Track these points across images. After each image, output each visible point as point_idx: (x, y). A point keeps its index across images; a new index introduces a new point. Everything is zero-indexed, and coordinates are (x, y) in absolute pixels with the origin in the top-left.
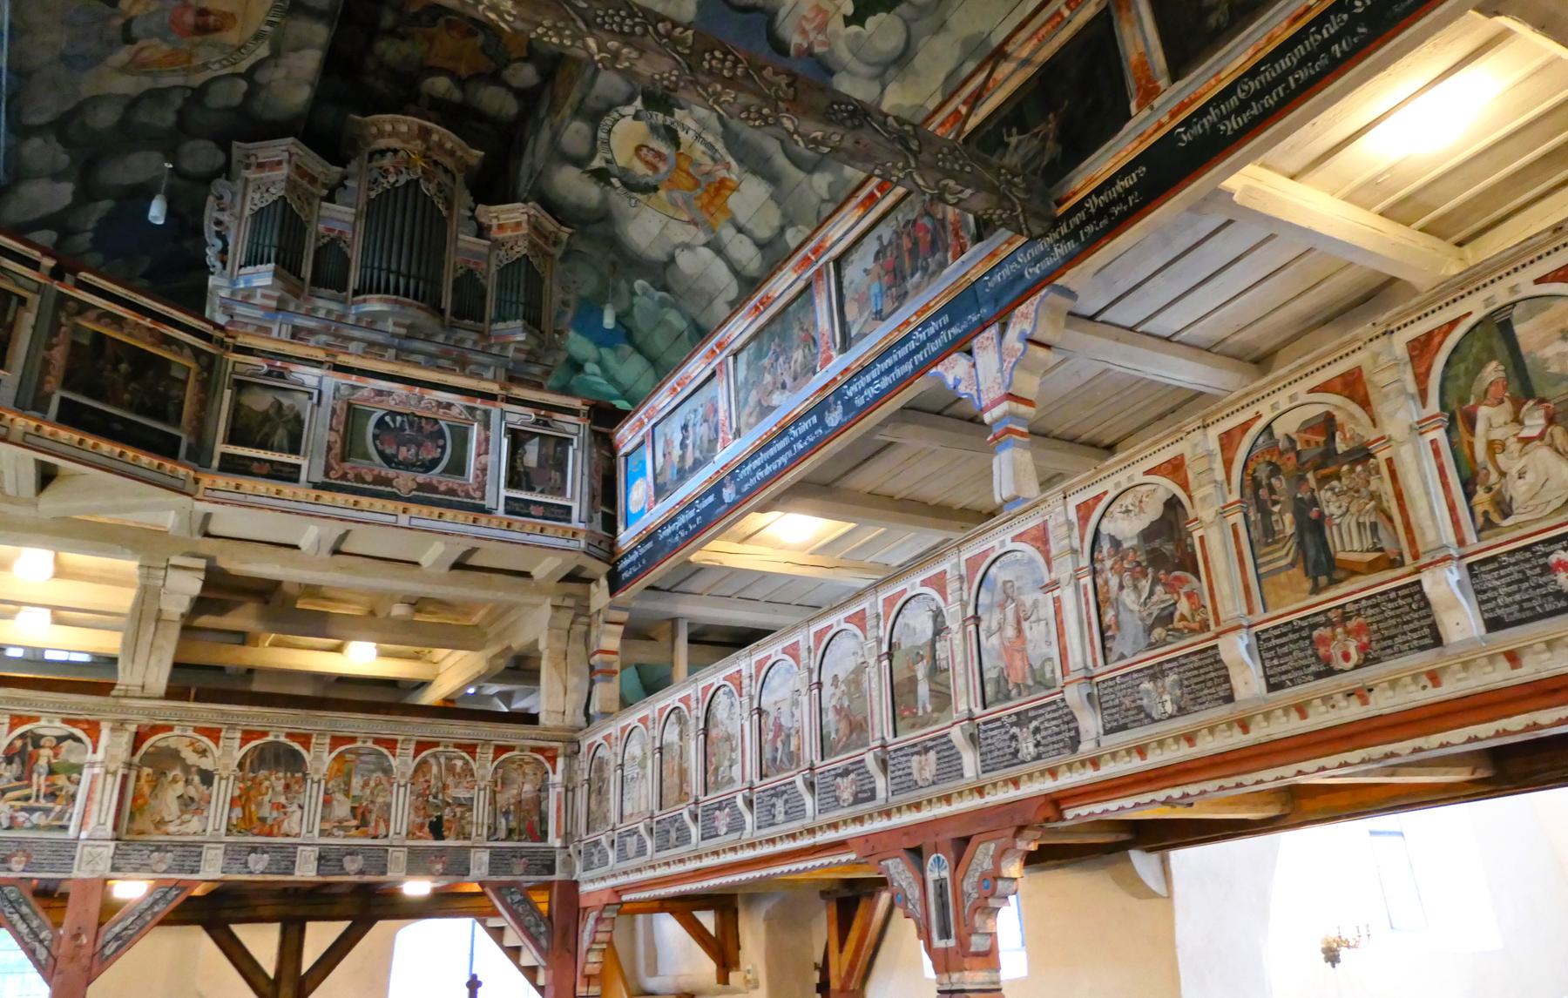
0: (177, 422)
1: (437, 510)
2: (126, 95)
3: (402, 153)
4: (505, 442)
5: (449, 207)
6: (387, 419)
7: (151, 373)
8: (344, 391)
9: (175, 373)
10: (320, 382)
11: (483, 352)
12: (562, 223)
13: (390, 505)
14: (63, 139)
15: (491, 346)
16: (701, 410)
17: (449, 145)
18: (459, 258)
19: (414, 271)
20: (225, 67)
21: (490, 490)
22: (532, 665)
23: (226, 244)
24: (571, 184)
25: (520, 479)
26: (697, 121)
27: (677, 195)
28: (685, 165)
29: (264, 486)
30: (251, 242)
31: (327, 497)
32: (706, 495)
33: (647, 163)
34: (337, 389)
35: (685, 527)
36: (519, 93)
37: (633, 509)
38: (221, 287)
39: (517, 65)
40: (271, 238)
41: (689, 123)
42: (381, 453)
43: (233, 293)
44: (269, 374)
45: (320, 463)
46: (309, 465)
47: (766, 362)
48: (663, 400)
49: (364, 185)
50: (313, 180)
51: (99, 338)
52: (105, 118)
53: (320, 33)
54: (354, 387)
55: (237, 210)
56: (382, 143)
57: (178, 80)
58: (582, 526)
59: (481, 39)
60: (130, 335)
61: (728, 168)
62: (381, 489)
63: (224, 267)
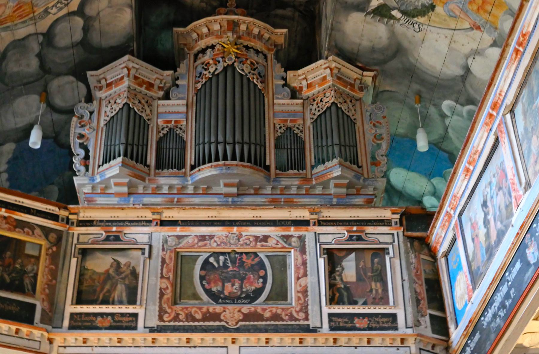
1: (263, 336)
3: (218, 47)
4: (321, 261)
5: (263, 78)
6: (212, 260)
7: (9, 254)
8: (172, 242)
9: (29, 251)
10: (150, 238)
11: (307, 194)
12: (363, 69)
15: (313, 187)
16: (494, 181)
17: (256, 31)
19: (238, 137)
20: (61, 9)
21: (313, 309)
23: (87, 151)
25: (341, 295)
29: (107, 337)
30: (106, 145)
31: (162, 338)
32: (512, 264)
34: (166, 241)
35: (502, 306)
37: (459, 306)
38: (83, 185)
40: (120, 139)
42: (208, 292)
43: (93, 188)
44: (107, 239)
45: (154, 309)
46: (146, 312)
48: (461, 185)
50: (150, 86)
54: (179, 237)
55: (94, 124)
56: (202, 44)
57: (30, 29)
58: (410, 331)
62: (211, 324)
63: (87, 170)
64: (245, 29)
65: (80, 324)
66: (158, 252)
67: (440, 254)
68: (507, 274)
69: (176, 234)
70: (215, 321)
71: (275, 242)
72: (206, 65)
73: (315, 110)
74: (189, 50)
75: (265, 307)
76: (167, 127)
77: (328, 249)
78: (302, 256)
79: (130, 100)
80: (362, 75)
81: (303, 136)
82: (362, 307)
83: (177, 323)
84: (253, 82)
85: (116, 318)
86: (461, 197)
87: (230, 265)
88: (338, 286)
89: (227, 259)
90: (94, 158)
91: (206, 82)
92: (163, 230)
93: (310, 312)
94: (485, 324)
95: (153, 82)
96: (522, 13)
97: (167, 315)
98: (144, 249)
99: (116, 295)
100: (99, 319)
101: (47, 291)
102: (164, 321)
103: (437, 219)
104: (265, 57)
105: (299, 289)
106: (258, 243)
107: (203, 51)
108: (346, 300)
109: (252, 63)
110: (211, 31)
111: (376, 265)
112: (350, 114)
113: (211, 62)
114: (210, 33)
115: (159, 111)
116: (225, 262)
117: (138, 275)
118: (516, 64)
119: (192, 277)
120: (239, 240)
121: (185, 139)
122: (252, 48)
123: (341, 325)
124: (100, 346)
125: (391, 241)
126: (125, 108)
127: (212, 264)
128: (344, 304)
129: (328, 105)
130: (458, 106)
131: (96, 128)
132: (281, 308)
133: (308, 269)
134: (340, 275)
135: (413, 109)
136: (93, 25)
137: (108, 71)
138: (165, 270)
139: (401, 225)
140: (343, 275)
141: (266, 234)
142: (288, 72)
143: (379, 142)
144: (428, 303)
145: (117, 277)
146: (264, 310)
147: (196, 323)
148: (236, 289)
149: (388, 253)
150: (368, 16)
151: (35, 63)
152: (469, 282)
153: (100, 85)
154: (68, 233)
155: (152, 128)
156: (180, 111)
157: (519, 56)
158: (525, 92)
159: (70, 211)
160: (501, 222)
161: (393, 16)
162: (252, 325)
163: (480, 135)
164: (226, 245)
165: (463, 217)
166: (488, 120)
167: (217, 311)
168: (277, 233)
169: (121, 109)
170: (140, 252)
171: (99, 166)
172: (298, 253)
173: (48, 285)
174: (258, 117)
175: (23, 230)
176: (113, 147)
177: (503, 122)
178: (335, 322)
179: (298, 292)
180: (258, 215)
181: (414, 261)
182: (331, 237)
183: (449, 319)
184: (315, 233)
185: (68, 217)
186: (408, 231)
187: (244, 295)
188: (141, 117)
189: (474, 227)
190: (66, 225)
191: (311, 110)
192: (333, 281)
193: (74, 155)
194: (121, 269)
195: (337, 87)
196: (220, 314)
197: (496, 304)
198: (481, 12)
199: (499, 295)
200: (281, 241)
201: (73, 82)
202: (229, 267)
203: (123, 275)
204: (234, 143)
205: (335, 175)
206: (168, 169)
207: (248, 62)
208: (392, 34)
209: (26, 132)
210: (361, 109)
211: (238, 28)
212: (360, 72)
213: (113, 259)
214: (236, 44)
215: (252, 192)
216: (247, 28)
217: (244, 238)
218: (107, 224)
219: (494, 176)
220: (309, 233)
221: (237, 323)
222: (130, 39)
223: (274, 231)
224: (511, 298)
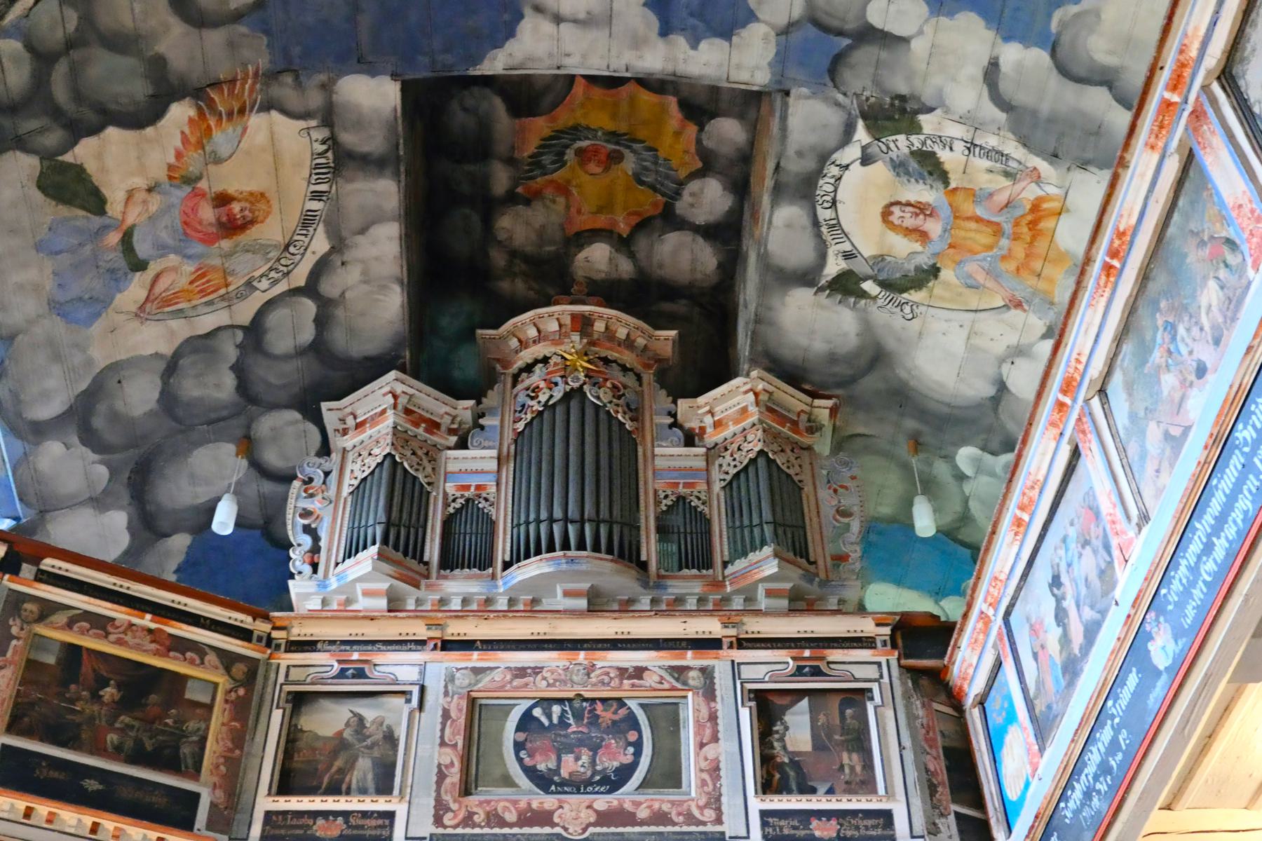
0: (195, 773)
2: (157, 355)
3: (555, 359)
4: (745, 714)
5: (636, 413)
6: (537, 712)
7: (153, 698)
9: (194, 693)
10: (423, 673)
12: (814, 395)
14: (90, 438)
16: (1072, 532)
17: (622, 333)
20: (275, 282)
21: (731, 804)
23: (316, 539)
24: (810, 322)
25: (785, 777)
26: (961, 121)
27: (971, 267)
28: (968, 208)
32: (1119, 681)
33: (909, 232)
34: (451, 679)
35: (1104, 769)
36: (710, 232)
37: (1012, 794)
38: (307, 596)
39: (694, 186)
41: (955, 131)
42: (531, 773)
43: (324, 602)
44: (342, 674)
45: (426, 804)
47: (1157, 356)
49: (509, 418)
50: (433, 426)
51: (73, 652)
52: (140, 396)
53: (386, 192)
54: (477, 671)
55: (332, 493)
56: (527, 356)
59: (629, 164)
60: (120, 642)
61: (1038, 179)
63: (315, 571)
66: (437, 699)
67: (969, 701)
68: (1110, 703)
69: (470, 665)
70: (542, 825)
71: (657, 678)
73: (729, 465)
76: (462, 496)
77: (756, 691)
79: (396, 449)
80: (811, 406)
81: (706, 510)
82: (824, 800)
83: (468, 831)
85: (352, 821)
86: (1008, 579)
87: (571, 721)
88: (778, 760)
90: (329, 550)
91: (533, 419)
93: (724, 808)
94: (1069, 815)
96: (1116, 193)
97: (450, 815)
98: (410, 693)
99: (355, 778)
100: (320, 822)
101: (223, 768)
102: (445, 827)
103: (961, 630)
104: (639, 378)
105: (704, 765)
107: (529, 368)
108: (794, 787)
109: (615, 387)
111: (849, 721)
112: (791, 472)
113: (542, 384)
114: (541, 337)
118: (1107, 295)
119: (499, 743)
120: (588, 675)
122: (615, 361)
125: (877, 676)
127: (537, 719)
128: (790, 792)
129: (752, 455)
130: (988, 457)
133: (720, 728)
134: (782, 740)
135: (906, 467)
138: (448, 731)
139: (894, 646)
140: (786, 738)
141: (640, 664)
142: (680, 401)
143: (846, 520)
144: (952, 793)
147: (506, 830)
149: (872, 699)
151: (230, 381)
152: (1032, 739)
154: (268, 665)
155: (436, 498)
156: (486, 469)
157: (1112, 279)
158: (1127, 348)
160: (1092, 607)
161: (865, 292)
162: (613, 834)
163: (1040, 450)
165: (1012, 619)
166: (1056, 416)
168: (661, 663)
169: (380, 465)
170: (399, 701)
171: (337, 564)
172: (701, 699)
173: (224, 757)
175: (184, 655)
176: (362, 531)
177: (1087, 412)
178: (774, 827)
179: (702, 771)
180: (626, 631)
181: (921, 712)
182: (764, 669)
183: (993, 822)
186: (907, 657)
187: (598, 778)
188: (415, 478)
189: (1034, 631)
191: (721, 466)
197: (1091, 769)
198: (1024, 274)
199: (1094, 749)
201: (297, 422)
203: (369, 742)
204: (582, 522)
206: (462, 568)
207: (609, 384)
208: (867, 327)
209: (210, 510)
210: (813, 476)
212: (809, 399)
214: (586, 354)
215: (616, 607)
216: (607, 328)
217: (598, 672)
218: (343, 648)
219: (1072, 524)
220: (720, 663)
221: (584, 830)
222: (398, 344)
224: (1120, 748)
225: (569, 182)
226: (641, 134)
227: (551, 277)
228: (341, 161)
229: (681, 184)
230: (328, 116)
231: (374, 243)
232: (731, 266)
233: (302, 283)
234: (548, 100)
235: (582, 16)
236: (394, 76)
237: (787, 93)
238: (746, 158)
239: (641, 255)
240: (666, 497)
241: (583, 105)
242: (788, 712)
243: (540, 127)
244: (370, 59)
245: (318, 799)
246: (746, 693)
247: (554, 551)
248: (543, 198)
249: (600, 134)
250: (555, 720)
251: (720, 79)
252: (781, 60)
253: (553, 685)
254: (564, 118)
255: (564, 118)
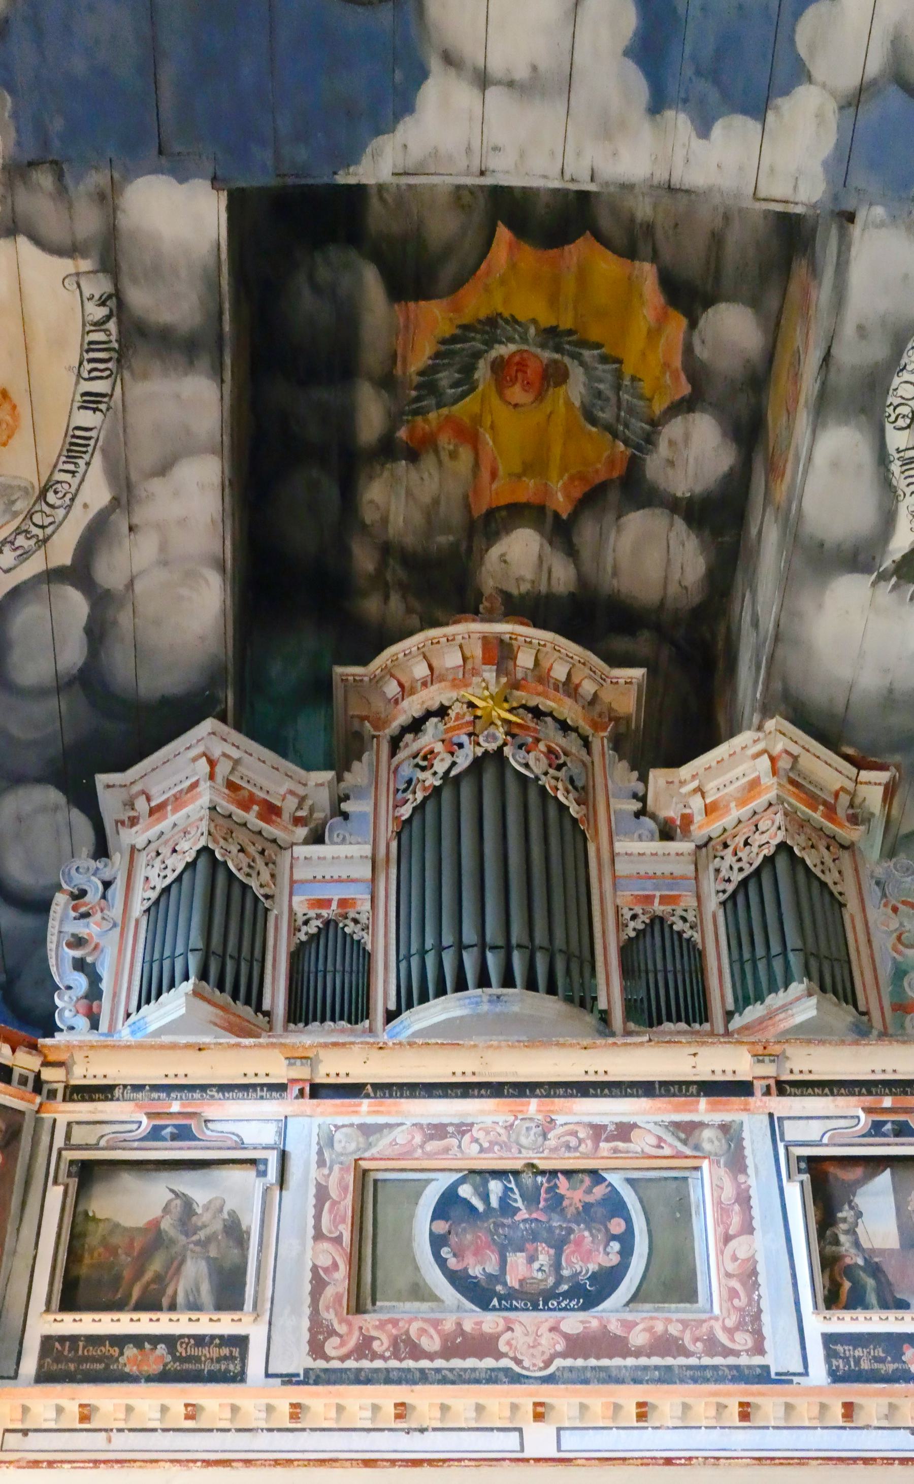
1: (629, 1397)
3: (457, 709)
4: (794, 1192)
5: (584, 795)
6: (465, 1191)
10: (283, 1133)
12: (859, 764)
13: (497, 1400)
17: (560, 672)
18: (625, 897)
20: (25, 555)
22: (571, 196)
23: (95, 979)
29: (149, 1402)
31: (320, 1401)
39: (674, 429)
44: (155, 1134)
45: (295, 1328)
46: (273, 1331)
50: (270, 811)
54: (367, 1130)
55: (116, 912)
56: (412, 707)
59: (576, 388)
62: (469, 1359)
64: (530, 664)
65: (72, 1367)
66: (307, 1172)
69: (357, 1120)
70: (481, 1357)
72: (425, 758)
73: (733, 868)
74: (376, 728)
75: (629, 1317)
76: (318, 916)
77: (811, 1160)
78: (736, 1178)
79: (215, 841)
81: (697, 937)
83: (365, 1364)
84: (556, 798)
88: (848, 1261)
89: (511, 1190)
90: (115, 995)
91: (425, 799)
92: (319, 1110)
93: (766, 1331)
95: (279, 804)
97: (335, 1341)
98: (265, 1162)
99: (181, 1288)
100: (130, 1351)
102: (327, 1359)
106: (603, 1145)
107: (416, 726)
109: (550, 751)
110: (436, 673)
112: (828, 879)
114: (434, 675)
115: (295, 877)
116: (504, 1200)
117: (248, 1233)
120: (545, 1136)
121: (369, 947)
122: (550, 714)
123: (865, 1365)
124: (131, 1430)
126: (202, 864)
129: (767, 851)
131: (119, 922)
132: (678, 1321)
133: (755, 1212)
134: (852, 1232)
136: (115, 623)
137: (153, 770)
141: (625, 1119)
145: (182, 1239)
146: (629, 1326)
147: (424, 1364)
148: (540, 1270)
150: (882, 583)
153: (132, 814)
154: (38, 1121)
156: (354, 875)
159: (45, 1057)
164: (509, 1149)
167: (487, 1328)
168: (658, 1118)
169: (191, 866)
170: (249, 1174)
171: (128, 1015)
172: (722, 1171)
174: (572, 891)
176: (167, 964)
178: (846, 1359)
179: (728, 1275)
184: (771, 1115)
185: (38, 1075)
187: (565, 1287)
188: (245, 887)
190: (31, 1096)
191: (718, 871)
192: (829, 1249)
193: (58, 988)
194: (194, 1219)
195: (790, 804)
196: (495, 1338)
200: (670, 1139)
201: (56, 808)
202: (519, 1209)
203: (202, 1235)
204: (508, 949)
205: (799, 1019)
207: (542, 746)
210: (856, 870)
211: (511, 663)
212: (852, 770)
213: (172, 1191)
217: (559, 1131)
218: (155, 1095)
220: (751, 1118)
221: (548, 1363)
222: (215, 677)
223: (645, 1113)
225: (477, 420)
226: (594, 335)
227: (444, 585)
228: (130, 340)
229: (655, 424)
230: (110, 253)
231: (176, 494)
232: (729, 561)
233: (67, 560)
234: (448, 271)
235: (521, 73)
236: (216, 181)
237: (851, 217)
238: (759, 379)
239: (586, 554)
240: (634, 917)
241: (503, 282)
242: (860, 1191)
243: (435, 318)
244: (177, 148)
245: (125, 1317)
246: (794, 1163)
247: (466, 988)
248: (437, 452)
249: (532, 331)
250: (494, 1203)
251: (738, 195)
252: (842, 164)
253: (490, 1150)
254: (475, 303)
255: (475, 303)
